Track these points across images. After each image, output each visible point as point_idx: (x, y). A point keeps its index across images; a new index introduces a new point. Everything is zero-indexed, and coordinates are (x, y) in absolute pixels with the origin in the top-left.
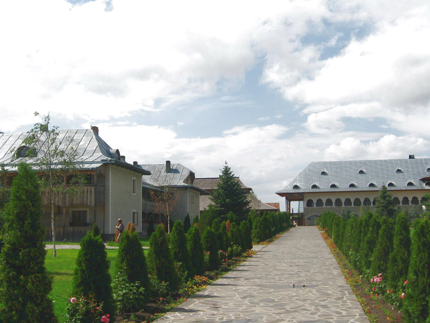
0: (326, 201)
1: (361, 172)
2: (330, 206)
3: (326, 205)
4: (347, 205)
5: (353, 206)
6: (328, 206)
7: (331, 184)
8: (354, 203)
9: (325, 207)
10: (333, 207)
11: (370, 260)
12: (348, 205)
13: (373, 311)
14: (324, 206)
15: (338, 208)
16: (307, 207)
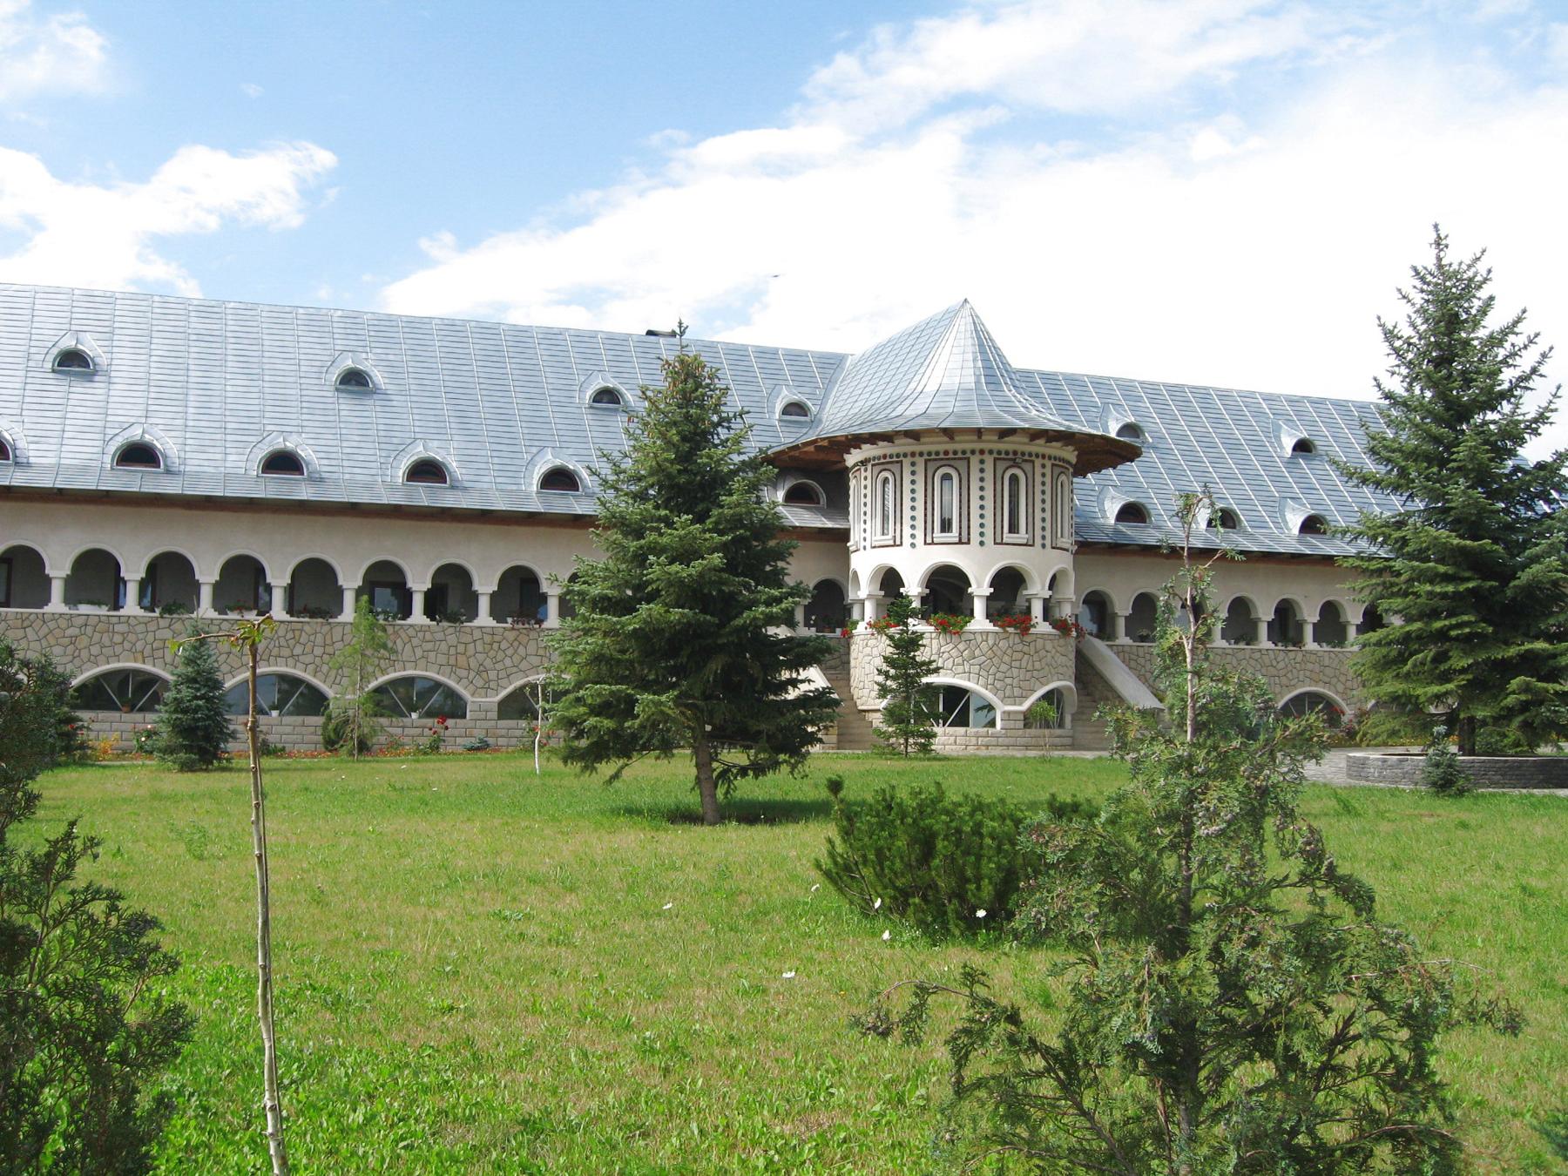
0: (295, 575)
1: (354, 380)
2: (99, 603)
3: (71, 599)
4: (232, 609)
5: (278, 611)
6: (84, 609)
7: (119, 441)
8: (291, 591)
9: (64, 609)
10: (122, 612)
11: (930, 827)
12: (240, 608)
13: (1225, 798)
14: (56, 605)
15: (163, 623)
16: (287, 617)
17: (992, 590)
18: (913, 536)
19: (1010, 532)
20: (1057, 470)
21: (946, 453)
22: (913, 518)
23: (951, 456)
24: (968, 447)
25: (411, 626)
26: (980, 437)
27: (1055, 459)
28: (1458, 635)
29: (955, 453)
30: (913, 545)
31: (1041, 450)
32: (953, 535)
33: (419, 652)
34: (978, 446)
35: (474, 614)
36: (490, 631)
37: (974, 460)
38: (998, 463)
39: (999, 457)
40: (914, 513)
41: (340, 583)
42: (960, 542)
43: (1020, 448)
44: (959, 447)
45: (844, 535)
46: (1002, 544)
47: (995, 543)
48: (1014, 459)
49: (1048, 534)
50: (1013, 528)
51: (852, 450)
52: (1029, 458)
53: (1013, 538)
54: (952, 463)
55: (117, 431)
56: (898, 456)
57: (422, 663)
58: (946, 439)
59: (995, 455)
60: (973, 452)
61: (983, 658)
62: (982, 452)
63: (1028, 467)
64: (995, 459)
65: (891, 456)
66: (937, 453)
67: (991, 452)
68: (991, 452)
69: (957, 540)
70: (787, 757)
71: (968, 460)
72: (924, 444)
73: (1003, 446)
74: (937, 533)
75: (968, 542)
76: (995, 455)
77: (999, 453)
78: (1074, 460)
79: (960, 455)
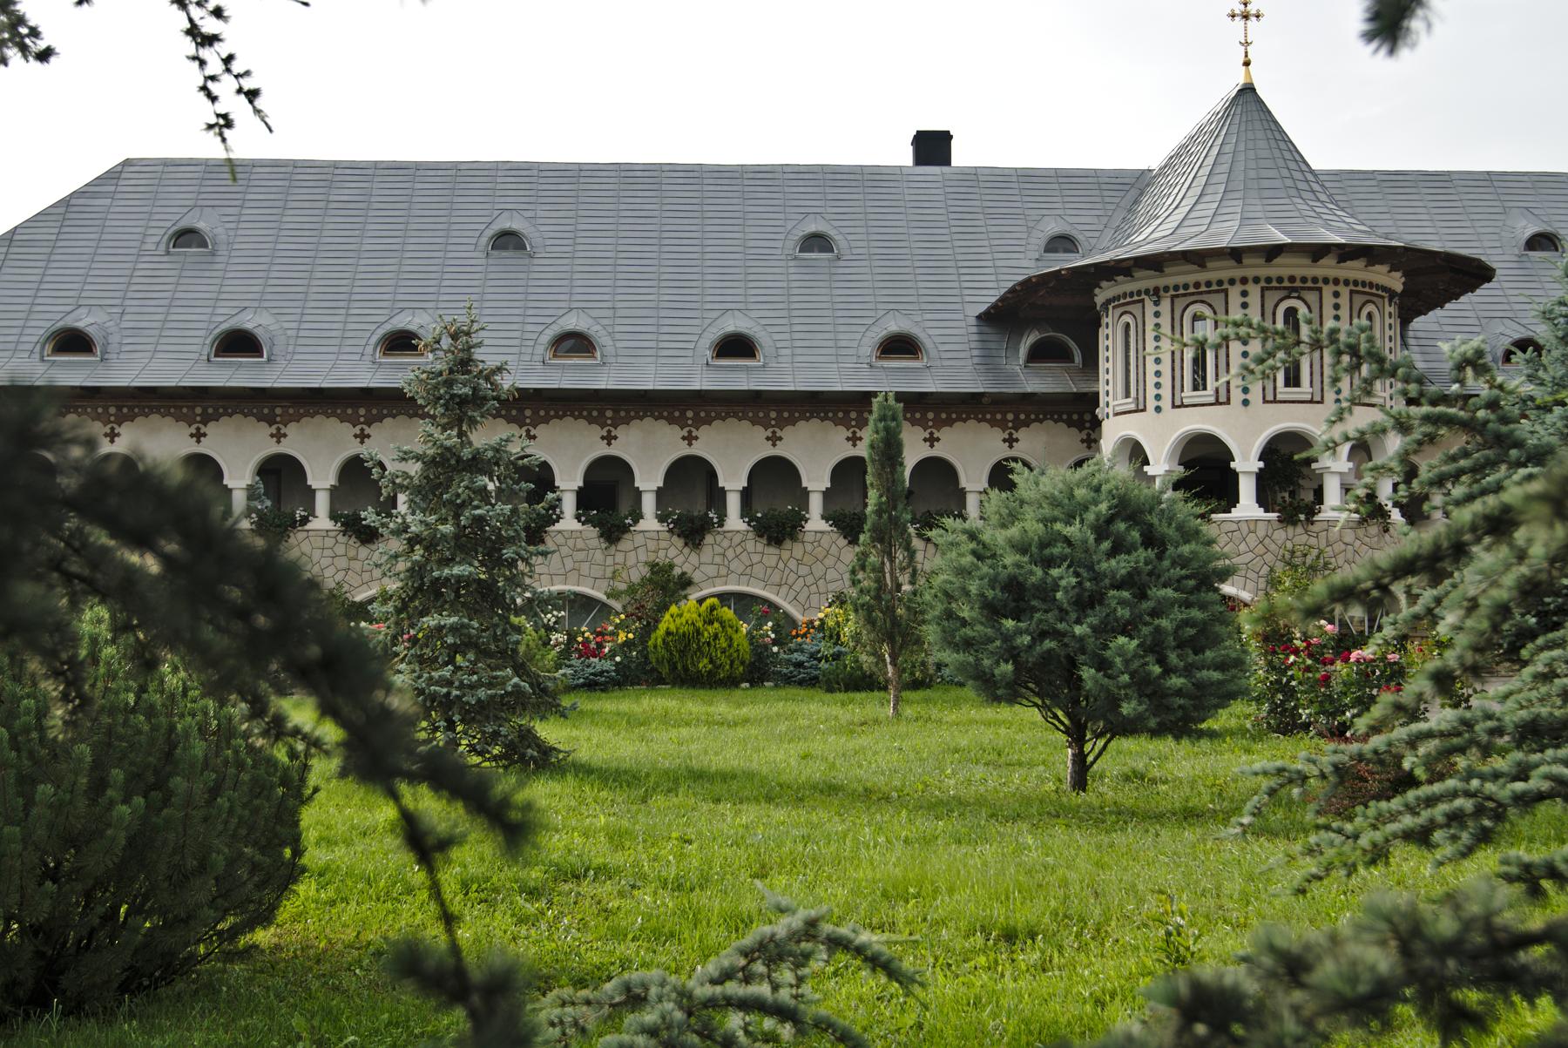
17: (1261, 464)
18: (1158, 397)
19: (1287, 384)
20: (1359, 300)
21: (1197, 285)
22: (1158, 374)
23: (1203, 289)
24: (1224, 275)
25: (560, 532)
26: (1239, 261)
27: (1356, 283)
28: (105, 550)
29: (1208, 284)
30: (1158, 409)
31: (1332, 273)
32: (1208, 395)
33: (569, 563)
34: (1238, 273)
35: (1232, 500)
36: (654, 535)
37: (1328, 291)
38: (1267, 293)
39: (1268, 284)
40: (1159, 368)
41: (804, 484)
42: (1217, 403)
43: (1298, 272)
44: (1213, 276)
45: (1093, 400)
46: (1275, 401)
47: (1265, 401)
48: (1293, 288)
49: (1166, 380)
50: (1199, 384)
51: (1104, 284)
52: (1316, 285)
53: (1293, 393)
54: (1204, 297)
55: (69, 308)
56: (1139, 293)
57: (573, 576)
58: (1232, 263)
59: (1263, 284)
60: (1232, 282)
61: (1251, 555)
62: (1244, 281)
63: (1312, 297)
64: (1263, 289)
65: (1132, 294)
66: (1186, 286)
67: (1256, 280)
68: (1256, 280)
69: (1212, 400)
70: (1530, 646)
71: (1226, 292)
72: (1167, 276)
73: (1272, 271)
74: (1188, 392)
75: (1228, 402)
76: (1263, 284)
77: (1269, 280)
78: (1399, 287)
79: (1215, 287)
